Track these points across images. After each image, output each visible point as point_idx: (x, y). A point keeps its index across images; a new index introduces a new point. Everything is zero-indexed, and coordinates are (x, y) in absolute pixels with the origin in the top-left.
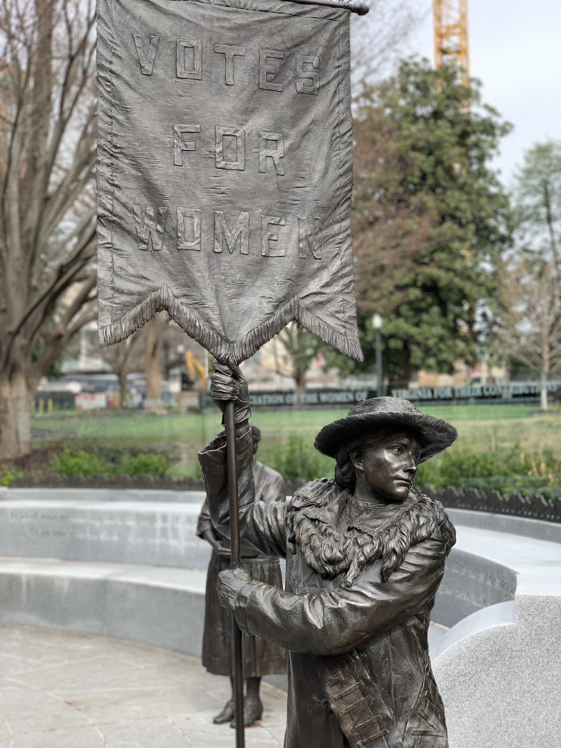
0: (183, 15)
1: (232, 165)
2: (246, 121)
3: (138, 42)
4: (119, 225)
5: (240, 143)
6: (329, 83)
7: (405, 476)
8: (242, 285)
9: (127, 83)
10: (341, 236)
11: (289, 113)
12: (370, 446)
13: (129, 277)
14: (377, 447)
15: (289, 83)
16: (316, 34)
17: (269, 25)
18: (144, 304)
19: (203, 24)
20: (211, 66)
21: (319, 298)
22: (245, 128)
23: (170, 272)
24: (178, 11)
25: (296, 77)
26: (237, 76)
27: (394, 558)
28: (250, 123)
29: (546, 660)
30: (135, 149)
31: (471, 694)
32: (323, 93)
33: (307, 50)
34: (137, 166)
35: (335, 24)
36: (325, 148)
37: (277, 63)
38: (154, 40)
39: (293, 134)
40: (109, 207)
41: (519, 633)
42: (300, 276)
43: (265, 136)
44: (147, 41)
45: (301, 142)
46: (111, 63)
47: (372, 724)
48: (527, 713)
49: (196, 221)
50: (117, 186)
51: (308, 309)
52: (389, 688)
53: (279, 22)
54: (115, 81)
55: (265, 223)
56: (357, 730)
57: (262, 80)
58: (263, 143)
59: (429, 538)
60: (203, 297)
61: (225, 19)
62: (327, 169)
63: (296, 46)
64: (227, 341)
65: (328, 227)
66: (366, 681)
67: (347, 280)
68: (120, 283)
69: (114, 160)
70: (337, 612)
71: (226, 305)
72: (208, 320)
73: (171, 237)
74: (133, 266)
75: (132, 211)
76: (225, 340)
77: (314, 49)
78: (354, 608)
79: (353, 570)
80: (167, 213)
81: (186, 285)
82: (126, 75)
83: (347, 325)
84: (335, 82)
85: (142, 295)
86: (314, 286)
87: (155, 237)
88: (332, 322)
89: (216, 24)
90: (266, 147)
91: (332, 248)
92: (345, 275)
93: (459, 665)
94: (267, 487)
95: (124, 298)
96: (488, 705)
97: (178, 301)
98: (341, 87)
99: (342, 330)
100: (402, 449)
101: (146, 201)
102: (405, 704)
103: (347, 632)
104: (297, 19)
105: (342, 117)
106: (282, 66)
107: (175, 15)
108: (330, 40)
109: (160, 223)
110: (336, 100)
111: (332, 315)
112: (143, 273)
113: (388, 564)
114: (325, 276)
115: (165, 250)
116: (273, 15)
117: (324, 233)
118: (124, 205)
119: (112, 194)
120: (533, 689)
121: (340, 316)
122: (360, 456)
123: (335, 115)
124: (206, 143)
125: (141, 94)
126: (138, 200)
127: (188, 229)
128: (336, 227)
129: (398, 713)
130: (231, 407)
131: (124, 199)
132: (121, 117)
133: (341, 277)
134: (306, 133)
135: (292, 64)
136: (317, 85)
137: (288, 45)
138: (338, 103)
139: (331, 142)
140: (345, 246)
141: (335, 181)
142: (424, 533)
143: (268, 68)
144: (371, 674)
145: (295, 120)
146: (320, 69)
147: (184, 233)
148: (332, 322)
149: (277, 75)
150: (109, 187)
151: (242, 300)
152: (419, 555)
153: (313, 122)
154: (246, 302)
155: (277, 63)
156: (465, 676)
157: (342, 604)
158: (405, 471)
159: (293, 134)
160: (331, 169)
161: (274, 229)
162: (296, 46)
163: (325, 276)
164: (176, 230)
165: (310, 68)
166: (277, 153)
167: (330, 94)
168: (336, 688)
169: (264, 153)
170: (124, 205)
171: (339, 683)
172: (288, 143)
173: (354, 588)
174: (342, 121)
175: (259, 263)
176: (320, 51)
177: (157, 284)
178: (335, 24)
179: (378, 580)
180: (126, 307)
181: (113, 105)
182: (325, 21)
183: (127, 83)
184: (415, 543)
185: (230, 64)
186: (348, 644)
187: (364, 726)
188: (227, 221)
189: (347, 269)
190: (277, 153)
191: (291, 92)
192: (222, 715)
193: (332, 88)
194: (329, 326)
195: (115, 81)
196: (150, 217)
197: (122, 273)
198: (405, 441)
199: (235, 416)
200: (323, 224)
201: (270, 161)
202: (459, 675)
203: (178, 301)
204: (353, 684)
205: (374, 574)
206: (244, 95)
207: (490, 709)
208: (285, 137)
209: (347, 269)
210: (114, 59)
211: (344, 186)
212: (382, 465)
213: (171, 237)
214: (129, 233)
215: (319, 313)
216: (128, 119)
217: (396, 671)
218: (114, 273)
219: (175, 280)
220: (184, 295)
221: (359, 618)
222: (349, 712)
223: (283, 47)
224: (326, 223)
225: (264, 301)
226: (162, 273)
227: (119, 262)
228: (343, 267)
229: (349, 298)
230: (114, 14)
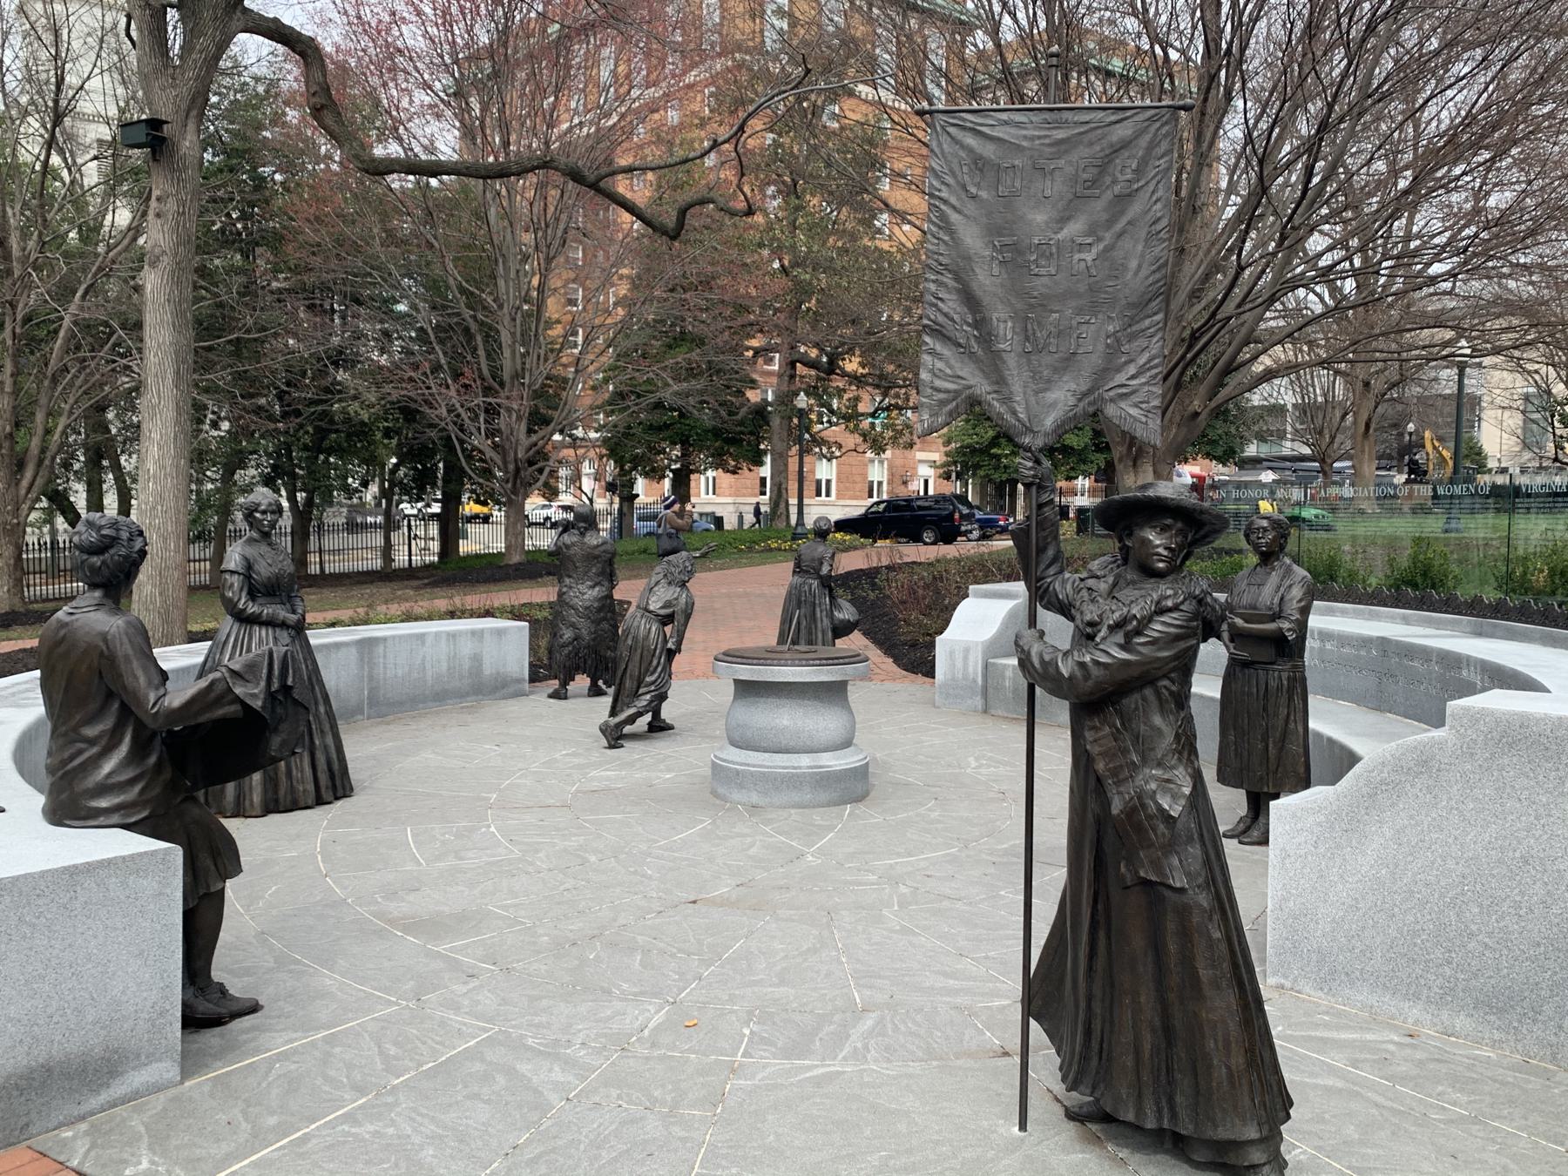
0: (1006, 137)
1: (1043, 271)
2: (1062, 229)
3: (965, 169)
4: (940, 332)
5: (1054, 250)
6: (1147, 183)
7: (1165, 553)
8: (1049, 381)
9: (954, 208)
10: (1152, 330)
11: (1105, 216)
12: (1137, 525)
13: (946, 377)
14: (1141, 527)
15: (1107, 188)
16: (1136, 138)
17: (1090, 135)
18: (959, 400)
19: (1025, 144)
20: (1031, 181)
21: (1124, 390)
22: (1059, 236)
23: (983, 371)
24: (1001, 135)
25: (1115, 182)
26: (1055, 188)
27: (1135, 623)
28: (1065, 231)
29: (1477, 777)
30: (958, 265)
31: (1393, 805)
32: (1141, 193)
33: (1127, 154)
34: (957, 278)
35: (1158, 124)
36: (1140, 248)
37: (1095, 171)
38: (980, 165)
39: (1108, 236)
40: (933, 317)
41: (1450, 744)
42: (1105, 370)
43: (1080, 240)
44: (973, 167)
45: (1116, 242)
46: (940, 191)
47: (1121, 766)
48: (1454, 832)
49: (1010, 324)
50: (940, 299)
51: (1112, 400)
52: (1138, 738)
53: (1099, 131)
54: (943, 207)
55: (1074, 323)
56: (1109, 770)
57: (1079, 189)
58: (1076, 248)
59: (1175, 608)
60: (1011, 393)
61: (1046, 136)
62: (1140, 266)
63: (1116, 151)
64: (1032, 431)
65: (1138, 322)
66: (1117, 729)
67: (1154, 371)
68: (938, 383)
69: (940, 277)
70: (1082, 665)
71: (1032, 400)
72: (1014, 413)
73: (986, 341)
74: (951, 367)
75: (952, 320)
76: (1029, 430)
77: (1134, 152)
78: (1097, 663)
79: (1103, 632)
80: (983, 319)
81: (997, 383)
82: (953, 200)
83: (1150, 415)
84: (1154, 182)
85: (957, 393)
86: (1120, 378)
87: (973, 342)
88: (1134, 412)
89: (1037, 142)
90: (1080, 252)
91: (1142, 342)
92: (1152, 368)
93: (1382, 772)
94: (1290, 586)
95: (942, 396)
96: (1411, 817)
97: (989, 397)
98: (1160, 186)
99: (1144, 419)
100: (1165, 529)
101: (966, 310)
102: (1152, 753)
103: (1090, 683)
104: (1118, 126)
105: (1159, 215)
106: (1100, 173)
107: (999, 139)
108: (1151, 141)
109: (977, 328)
110: (1154, 198)
111: (1136, 406)
112: (960, 373)
113: (1129, 628)
114: (1132, 370)
115: (980, 352)
116: (1093, 125)
117: (1134, 328)
118: (946, 315)
119: (936, 305)
120: (1462, 807)
121: (1143, 406)
122: (1130, 535)
123: (1152, 213)
124: (1020, 253)
125: (965, 216)
126: (958, 309)
127: (1001, 332)
128: (1147, 322)
129: (1144, 760)
130: (1034, 489)
131: (946, 309)
132: (946, 238)
133: (1148, 369)
134: (1120, 235)
135: (1110, 170)
136: (1136, 186)
137: (1107, 152)
138: (1156, 202)
139: (1146, 240)
140: (1155, 339)
141: (1147, 278)
142: (1170, 603)
143: (1085, 176)
144: (1123, 724)
145: (1110, 222)
146: (1138, 172)
147: (996, 336)
148: (1134, 412)
149: (1094, 183)
150: (934, 301)
151: (1048, 394)
152: (1164, 623)
153: (1129, 223)
154: (1052, 396)
155: (1095, 171)
156: (1388, 784)
157: (1087, 659)
158: (1166, 548)
159: (1108, 236)
160: (1145, 266)
161: (1084, 328)
162: (1116, 151)
163: (1132, 370)
164: (990, 334)
165: (1129, 170)
166: (1089, 257)
167: (1148, 195)
168: (1092, 733)
169: (1077, 256)
170: (946, 315)
171: (1094, 728)
172: (1101, 247)
173: (1101, 647)
174: (1159, 219)
175: (1067, 359)
176: (1140, 153)
177: (972, 383)
178: (1158, 124)
179: (1122, 641)
180: (942, 403)
181: (940, 227)
182: (1146, 124)
183: (954, 208)
184: (1162, 611)
185: (1049, 177)
186: (1091, 693)
187: (1115, 768)
188: (1039, 323)
189: (1156, 361)
190: (1089, 257)
191: (1108, 195)
192: (1232, 830)
193: (1151, 187)
194: (1130, 415)
195: (943, 207)
196: (969, 325)
197: (941, 374)
198: (1169, 521)
199: (1038, 497)
200: (1132, 321)
201: (1083, 264)
202: (1382, 782)
203: (989, 397)
204: (1107, 729)
205: (1119, 638)
206: (1060, 205)
207: (1413, 822)
208: (1099, 239)
209: (1156, 361)
210: (943, 187)
211: (1158, 281)
212: (1146, 543)
213: (986, 341)
214: (949, 339)
215: (1123, 405)
216: (952, 238)
217: (1145, 724)
218: (935, 375)
219: (987, 378)
220: (995, 392)
221: (1102, 672)
222: (1100, 754)
223: (1102, 154)
224: (1137, 318)
225: (1069, 394)
226: (976, 372)
227: (939, 365)
228: (1149, 361)
229: (1154, 389)
230: (945, 146)
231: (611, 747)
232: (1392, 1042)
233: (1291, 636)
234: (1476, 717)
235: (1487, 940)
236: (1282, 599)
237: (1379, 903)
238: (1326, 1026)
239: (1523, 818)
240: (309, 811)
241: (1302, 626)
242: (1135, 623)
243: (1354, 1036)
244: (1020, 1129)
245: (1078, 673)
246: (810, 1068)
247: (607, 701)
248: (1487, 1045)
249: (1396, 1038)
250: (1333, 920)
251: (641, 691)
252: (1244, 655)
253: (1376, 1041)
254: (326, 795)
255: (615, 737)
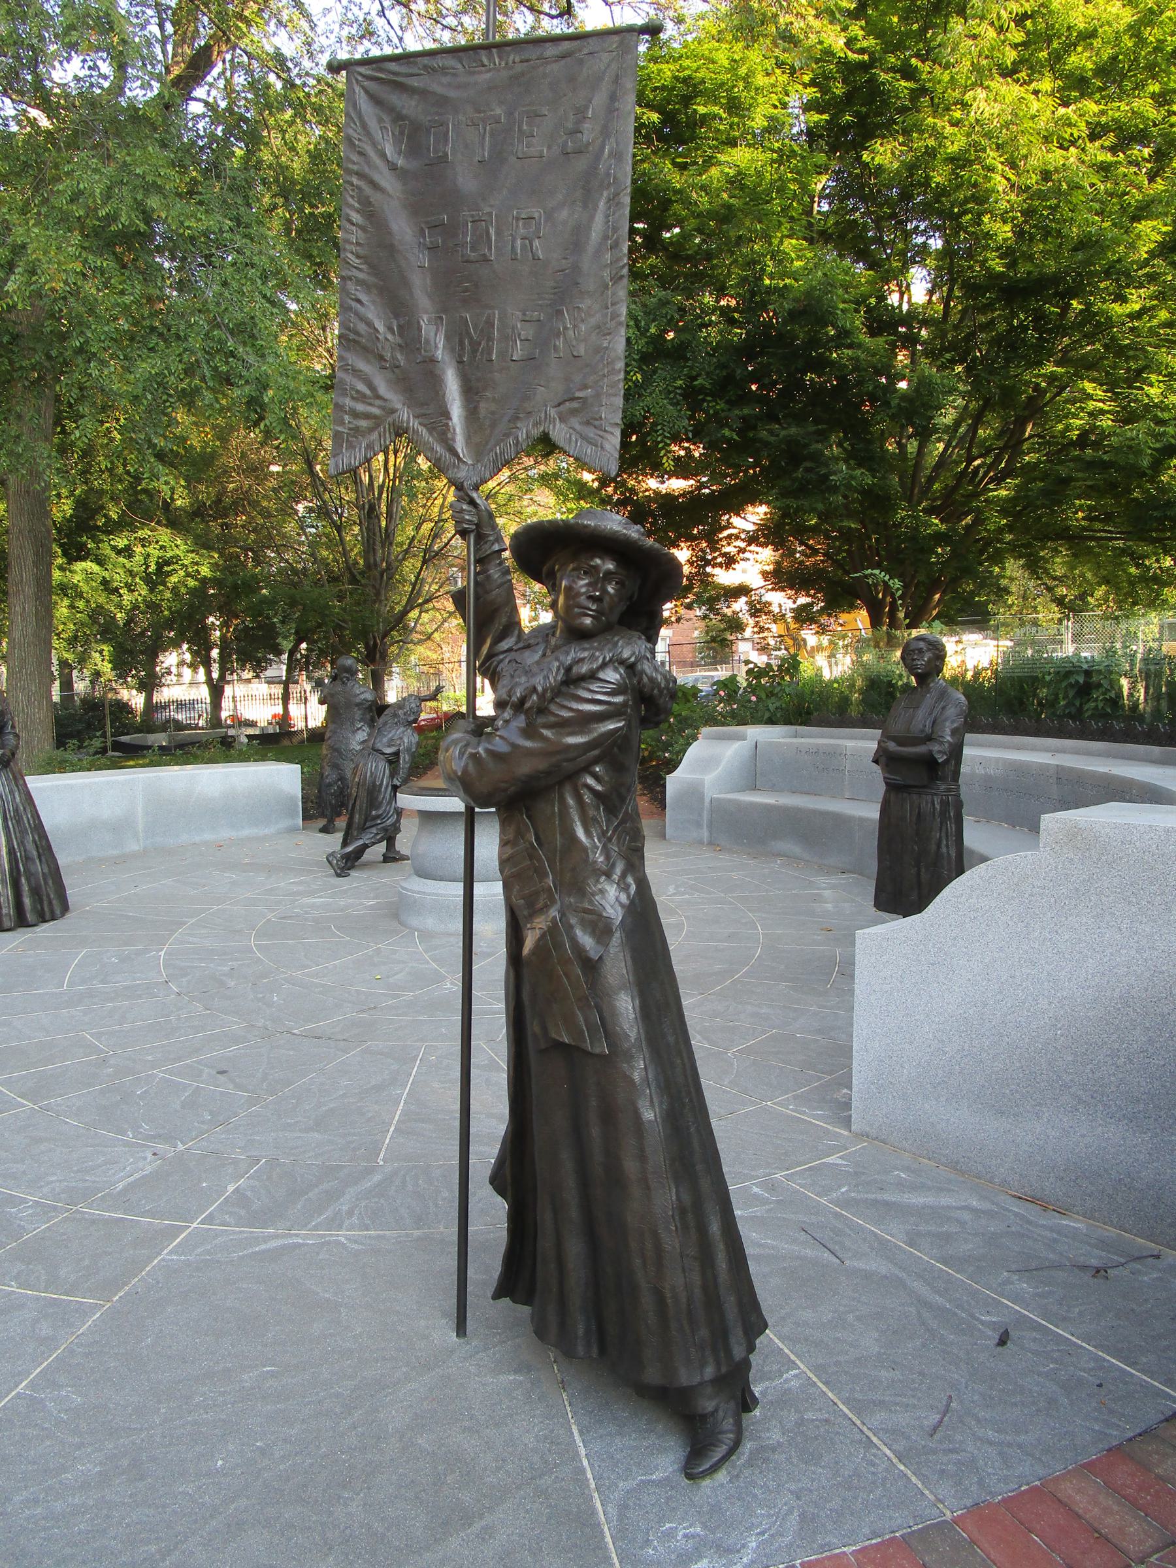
27: (535, 697)
70: (475, 757)
156: (976, 911)
231: (339, 876)
232: (967, 1208)
233: (941, 759)
234: (1074, 834)
235: (1080, 1093)
236: (934, 722)
237: (966, 1047)
238: (901, 1185)
239: (1124, 952)
240: (10, 933)
241: (956, 753)
242: (535, 697)
243: (922, 1200)
244: (458, 1335)
245: (471, 768)
246: (266, 1239)
247: (339, 836)
248: (1078, 1214)
249: (975, 1203)
250: (919, 1064)
251: (368, 824)
252: (898, 779)
253: (949, 1207)
254: (30, 917)
255: (348, 863)
